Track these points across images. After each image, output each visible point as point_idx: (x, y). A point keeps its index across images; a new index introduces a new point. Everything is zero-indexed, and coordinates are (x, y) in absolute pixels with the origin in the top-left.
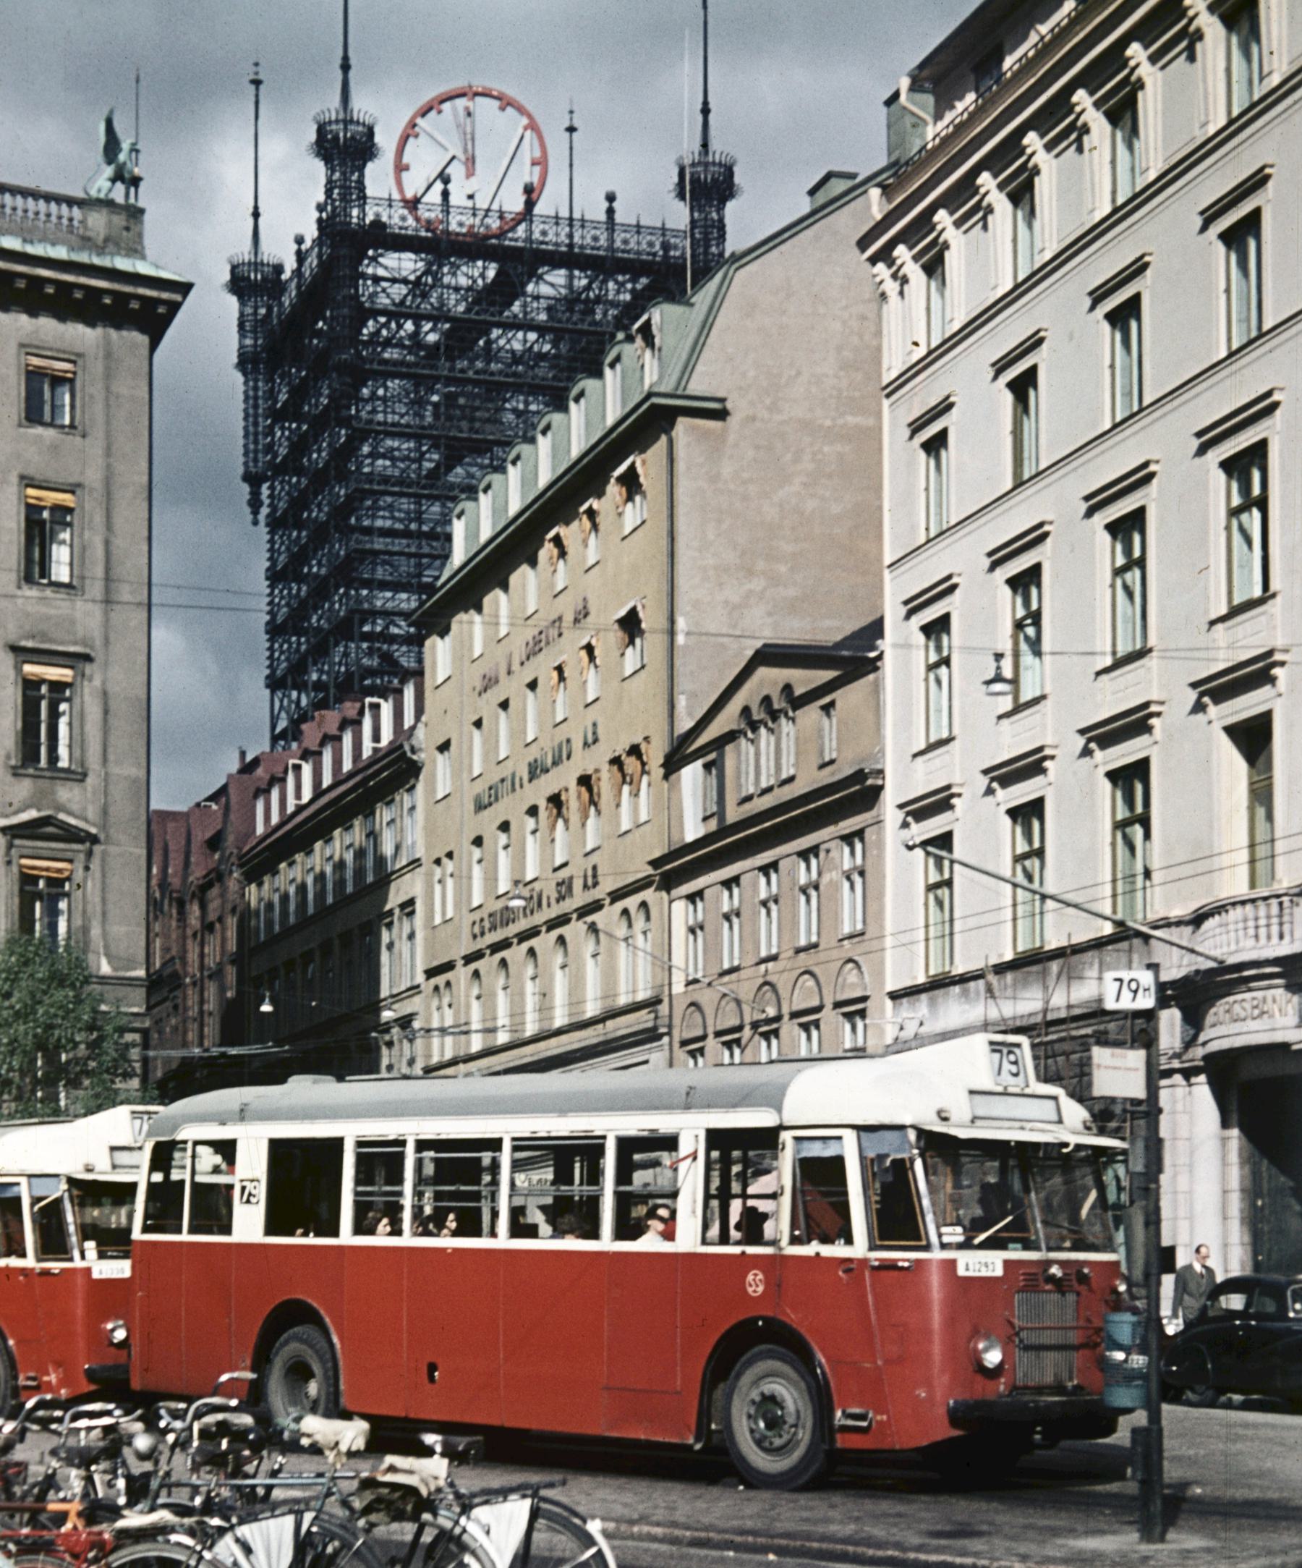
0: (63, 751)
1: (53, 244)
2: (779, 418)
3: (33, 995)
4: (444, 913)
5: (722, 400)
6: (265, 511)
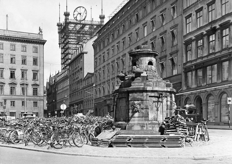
6: (61, 47)
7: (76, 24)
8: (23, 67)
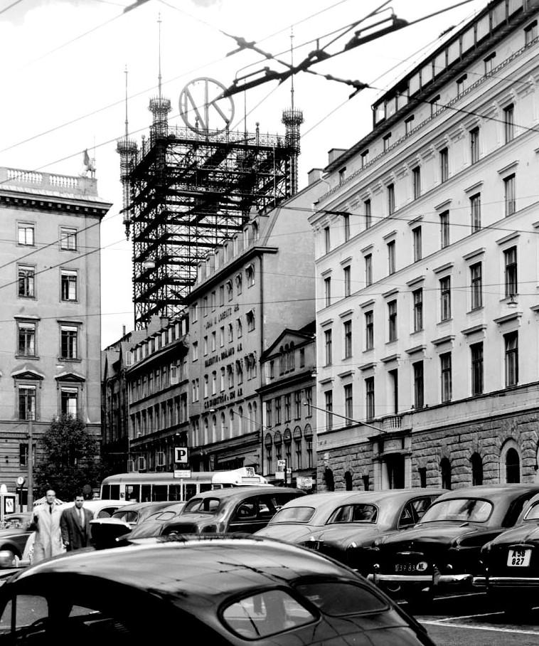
0: (74, 353)
1: (69, 193)
2: (295, 253)
3: (69, 432)
4: (196, 399)
5: (277, 249)
6: (131, 235)
7: (195, 145)
8: (22, 310)
